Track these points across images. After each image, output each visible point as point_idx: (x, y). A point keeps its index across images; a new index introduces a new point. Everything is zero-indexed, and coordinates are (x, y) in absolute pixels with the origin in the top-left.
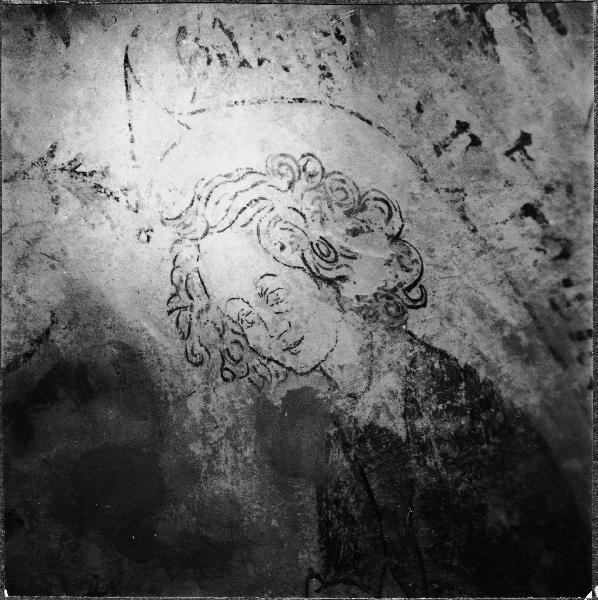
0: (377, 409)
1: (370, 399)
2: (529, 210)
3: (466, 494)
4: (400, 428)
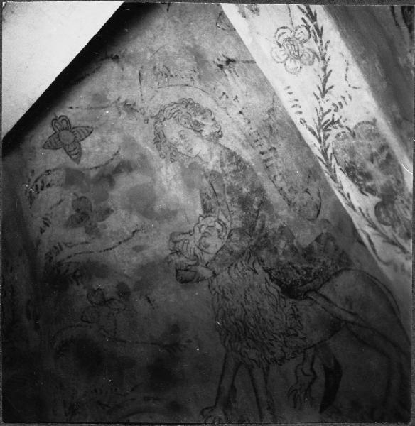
0: (214, 166)
1: (211, 163)
2: (241, 113)
3: (238, 186)
4: (220, 170)
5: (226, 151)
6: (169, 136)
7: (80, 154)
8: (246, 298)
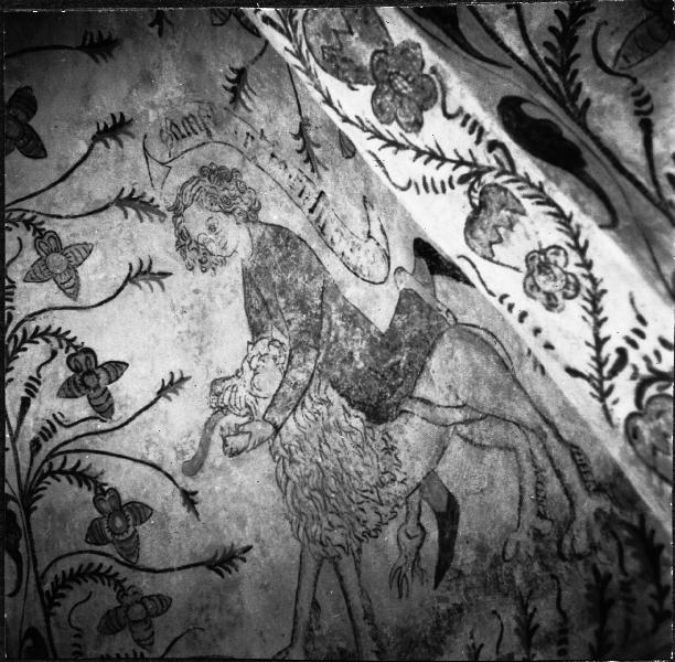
5: (270, 229)
6: (194, 233)
7: (77, 286)
8: (321, 451)
